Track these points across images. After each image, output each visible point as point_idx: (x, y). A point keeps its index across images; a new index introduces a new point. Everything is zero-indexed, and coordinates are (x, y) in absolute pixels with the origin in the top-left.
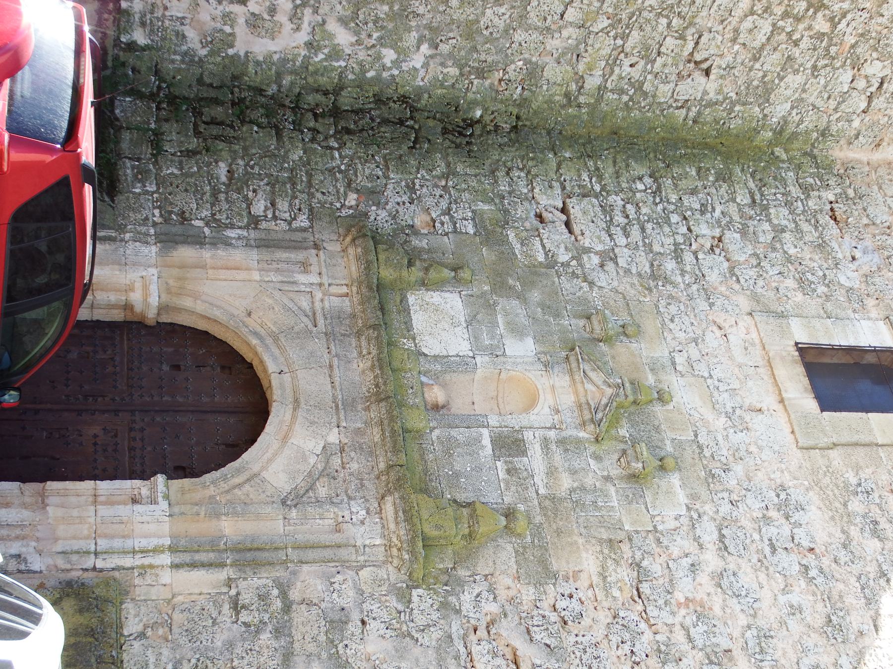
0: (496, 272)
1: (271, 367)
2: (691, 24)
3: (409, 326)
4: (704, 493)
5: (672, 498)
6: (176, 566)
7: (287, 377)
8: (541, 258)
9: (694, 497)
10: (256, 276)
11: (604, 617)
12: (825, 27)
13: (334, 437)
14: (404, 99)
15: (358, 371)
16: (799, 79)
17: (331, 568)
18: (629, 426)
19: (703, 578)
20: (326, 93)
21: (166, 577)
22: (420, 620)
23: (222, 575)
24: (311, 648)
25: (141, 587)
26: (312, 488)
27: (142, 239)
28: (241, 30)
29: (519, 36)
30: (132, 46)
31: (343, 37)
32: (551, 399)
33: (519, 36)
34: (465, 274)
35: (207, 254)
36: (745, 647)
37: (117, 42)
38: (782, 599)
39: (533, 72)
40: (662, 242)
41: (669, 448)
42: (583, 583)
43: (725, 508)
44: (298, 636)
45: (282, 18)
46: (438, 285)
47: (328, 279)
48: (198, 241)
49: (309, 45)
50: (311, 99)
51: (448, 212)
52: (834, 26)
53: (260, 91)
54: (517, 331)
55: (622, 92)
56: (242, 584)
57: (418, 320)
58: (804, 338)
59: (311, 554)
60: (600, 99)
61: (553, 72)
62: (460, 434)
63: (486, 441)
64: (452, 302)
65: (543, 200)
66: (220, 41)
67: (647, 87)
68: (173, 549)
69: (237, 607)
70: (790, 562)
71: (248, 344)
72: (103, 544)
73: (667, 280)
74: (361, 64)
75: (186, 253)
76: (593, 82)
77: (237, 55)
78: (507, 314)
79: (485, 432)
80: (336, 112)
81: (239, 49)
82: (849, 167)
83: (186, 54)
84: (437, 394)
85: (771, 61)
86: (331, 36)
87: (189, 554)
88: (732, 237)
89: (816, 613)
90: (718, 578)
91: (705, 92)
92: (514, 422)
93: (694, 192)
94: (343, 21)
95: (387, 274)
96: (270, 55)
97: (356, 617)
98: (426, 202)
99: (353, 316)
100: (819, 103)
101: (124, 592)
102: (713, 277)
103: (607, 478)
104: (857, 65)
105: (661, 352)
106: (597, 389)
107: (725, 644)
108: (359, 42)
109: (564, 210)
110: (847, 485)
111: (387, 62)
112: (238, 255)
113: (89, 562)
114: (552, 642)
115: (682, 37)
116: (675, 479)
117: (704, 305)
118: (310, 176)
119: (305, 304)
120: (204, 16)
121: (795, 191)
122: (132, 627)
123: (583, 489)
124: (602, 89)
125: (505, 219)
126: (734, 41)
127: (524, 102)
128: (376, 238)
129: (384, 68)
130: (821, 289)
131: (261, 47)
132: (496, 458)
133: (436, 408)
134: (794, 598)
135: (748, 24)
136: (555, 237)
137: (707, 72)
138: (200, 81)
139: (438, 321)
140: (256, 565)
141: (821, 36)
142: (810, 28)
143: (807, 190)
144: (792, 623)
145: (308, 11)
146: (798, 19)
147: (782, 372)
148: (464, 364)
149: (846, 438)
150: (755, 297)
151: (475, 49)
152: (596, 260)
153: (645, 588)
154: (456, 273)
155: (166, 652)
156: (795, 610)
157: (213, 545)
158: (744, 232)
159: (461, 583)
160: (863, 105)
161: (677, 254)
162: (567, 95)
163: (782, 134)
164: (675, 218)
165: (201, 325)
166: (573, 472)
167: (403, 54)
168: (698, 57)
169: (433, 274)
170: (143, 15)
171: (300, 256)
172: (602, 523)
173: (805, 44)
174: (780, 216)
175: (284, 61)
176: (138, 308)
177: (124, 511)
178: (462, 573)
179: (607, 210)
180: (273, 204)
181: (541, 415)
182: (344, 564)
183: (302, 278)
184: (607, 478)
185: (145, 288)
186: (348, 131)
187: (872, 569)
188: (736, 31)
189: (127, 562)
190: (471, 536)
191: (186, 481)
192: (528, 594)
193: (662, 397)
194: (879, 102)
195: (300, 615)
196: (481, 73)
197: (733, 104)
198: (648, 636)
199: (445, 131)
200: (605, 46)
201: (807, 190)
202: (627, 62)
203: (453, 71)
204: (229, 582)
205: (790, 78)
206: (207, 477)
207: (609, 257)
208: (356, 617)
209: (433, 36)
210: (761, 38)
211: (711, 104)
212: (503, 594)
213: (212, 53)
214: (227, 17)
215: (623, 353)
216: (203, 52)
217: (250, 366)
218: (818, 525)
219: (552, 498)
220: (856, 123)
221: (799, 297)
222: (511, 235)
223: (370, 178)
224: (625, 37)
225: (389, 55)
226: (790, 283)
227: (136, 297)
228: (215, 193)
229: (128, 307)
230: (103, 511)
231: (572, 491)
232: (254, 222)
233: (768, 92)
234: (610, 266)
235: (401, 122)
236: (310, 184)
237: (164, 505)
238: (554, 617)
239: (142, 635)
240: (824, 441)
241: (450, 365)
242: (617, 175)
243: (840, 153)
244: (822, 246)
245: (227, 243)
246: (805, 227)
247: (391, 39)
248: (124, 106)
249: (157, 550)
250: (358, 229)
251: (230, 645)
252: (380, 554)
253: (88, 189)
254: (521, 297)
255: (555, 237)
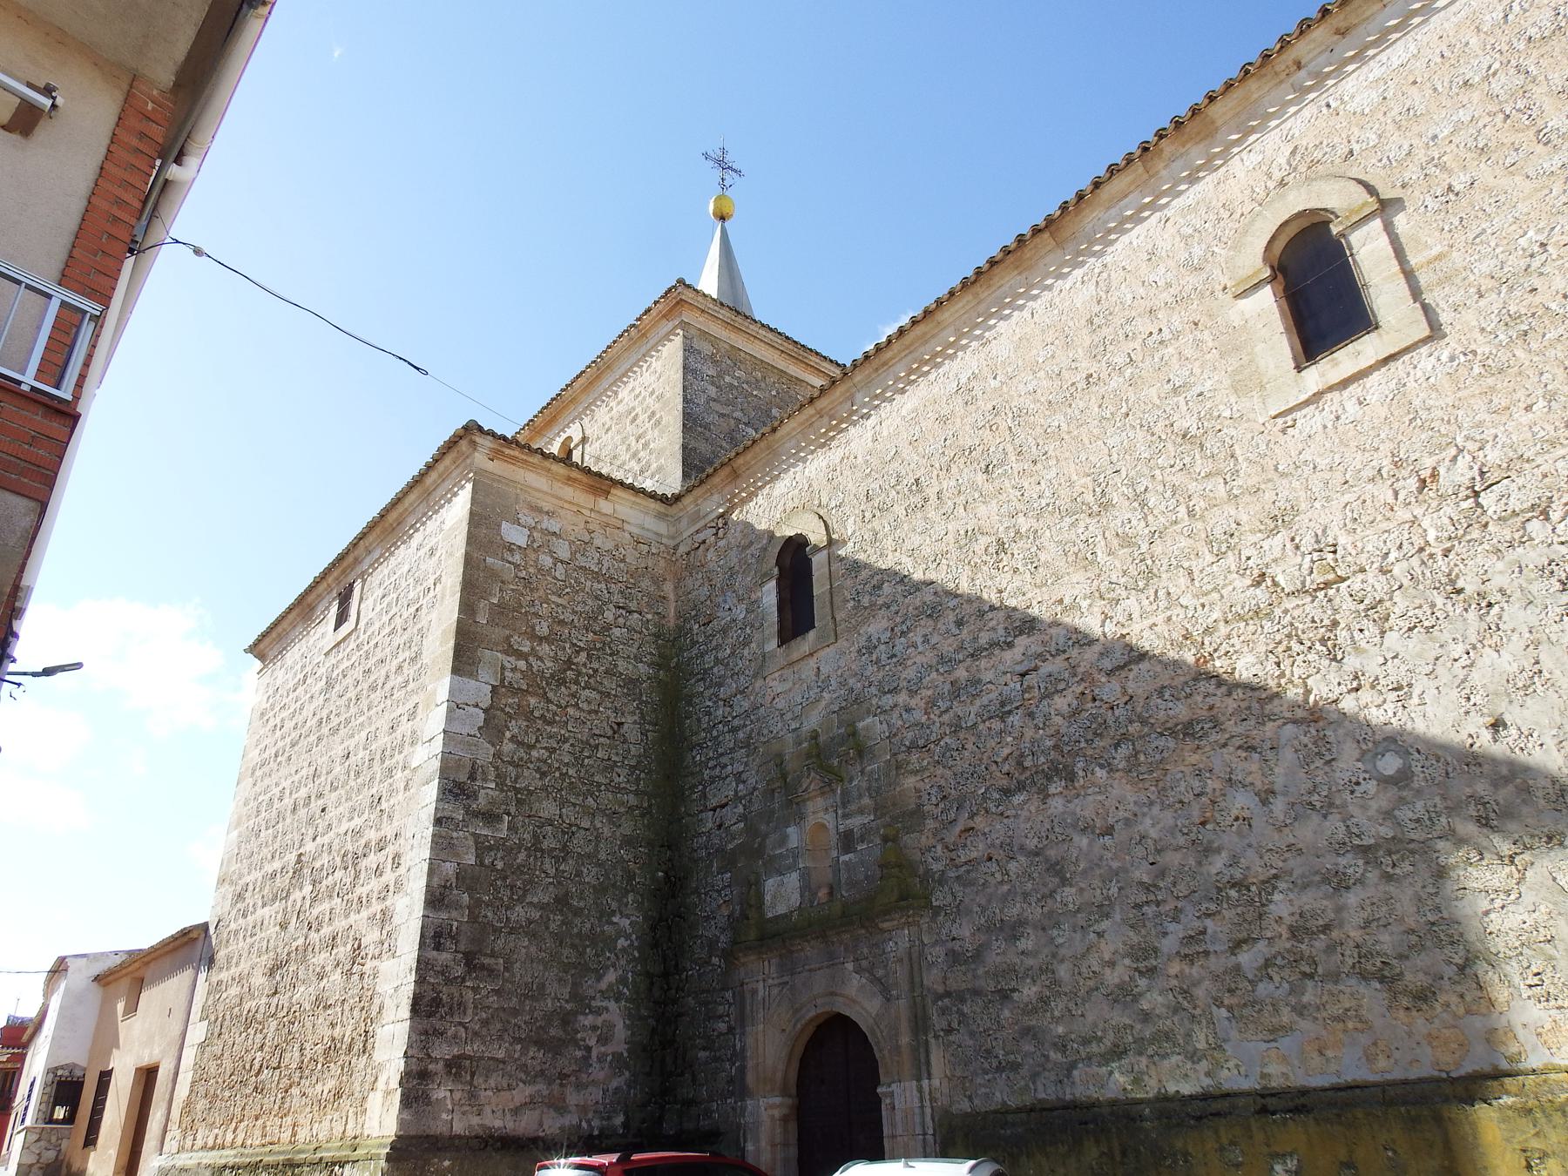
0: (751, 860)
1: (812, 1014)
2: (587, 743)
3: (785, 916)
4: (865, 706)
5: (872, 726)
6: (929, 1078)
7: (819, 1001)
8: (742, 825)
9: (868, 712)
10: (761, 1027)
11: (940, 771)
12: (583, 655)
13: (850, 966)
14: (653, 928)
15: (810, 950)
16: (620, 663)
17: (924, 964)
18: (834, 755)
19: (913, 703)
20: (652, 983)
21: (936, 1082)
22: (949, 898)
23: (932, 1041)
24: (969, 975)
25: (942, 1101)
26: (879, 980)
27: (743, 1109)
28: (609, 1049)
29: (603, 856)
30: (625, 1125)
31: (611, 977)
32: (820, 813)
33: (603, 856)
34: (752, 878)
35: (750, 1064)
36: (948, 672)
37: (623, 1136)
38: (921, 649)
39: (628, 842)
40: (728, 741)
41: (842, 730)
42: (920, 785)
43: (873, 690)
44: (964, 986)
45: (599, 1021)
46: (760, 896)
47: (761, 977)
48: (742, 1070)
49: (617, 1000)
50: (657, 993)
51: (719, 892)
52: (582, 649)
53: (654, 1031)
54: (784, 839)
55: (638, 779)
56: (937, 1027)
57: (781, 909)
58: (774, 643)
59: (917, 979)
60: (644, 793)
61: (627, 828)
62: (844, 876)
63: (846, 858)
64: (770, 884)
65: (710, 825)
66: (618, 1063)
67: (633, 763)
68: (919, 1080)
69: (950, 1031)
70: (901, 642)
71: (802, 1030)
72: (918, 1130)
73: (750, 737)
74: (629, 962)
75: (750, 1078)
76: (632, 800)
77: (628, 1050)
78: (774, 848)
79: (842, 858)
80: (666, 975)
81: (622, 1048)
82: (679, 616)
83: (629, 1087)
84: (822, 894)
85: (610, 684)
86: (610, 986)
87: (922, 1069)
88: (723, 692)
89: (926, 625)
90: (913, 693)
91: (635, 722)
92: (834, 838)
93: (699, 720)
94: (599, 979)
95: (753, 934)
96: (627, 1027)
97: (950, 945)
98: (715, 903)
99: (781, 956)
100: (636, 645)
101: (946, 1112)
102: (746, 705)
103: (862, 772)
104: (607, 628)
105: (790, 738)
106: (811, 782)
107: (948, 687)
108: (614, 965)
109: (714, 810)
110: (854, 608)
111: (626, 944)
112: (750, 1041)
113: (930, 1138)
114: (955, 806)
115: (597, 747)
116: (860, 725)
117: (762, 710)
118: (703, 992)
119: (775, 991)
120: (601, 1076)
121: (695, 651)
122: (965, 1106)
123: (869, 789)
124: (636, 793)
125: (720, 850)
126: (596, 712)
127: (650, 844)
128: (734, 942)
129: (631, 945)
130: (748, 631)
131: (621, 1032)
132: (855, 851)
133: (831, 894)
134: (919, 640)
135: (585, 706)
136: (731, 815)
137: (620, 724)
138: (649, 1074)
139: (783, 894)
140: (926, 1018)
141: (589, 657)
142: (585, 665)
143: (694, 643)
144: (933, 641)
145: (594, 1004)
146: (579, 674)
147: (795, 656)
148: (805, 876)
149: (828, 609)
150: (755, 676)
151: (614, 885)
152: (741, 786)
153: (921, 742)
154: (753, 887)
155: (979, 1080)
156: (926, 640)
157: (914, 1050)
158: (720, 685)
159: (928, 871)
160: (636, 616)
161: (734, 730)
162: (643, 815)
163: (661, 663)
164: (715, 733)
165: (795, 1065)
166: (860, 796)
167: (621, 933)
168: (610, 733)
169: (752, 902)
170: (603, 1119)
171: (748, 995)
172: (887, 775)
173: (595, 665)
174: (709, 659)
175: (630, 1016)
176: (785, 1111)
177: (899, 1116)
178: (921, 871)
179: (713, 780)
180: (721, 1017)
181: (828, 819)
182: (921, 954)
183: (761, 993)
184: (862, 772)
185: (772, 1107)
186: (677, 965)
187: (900, 588)
188: (590, 712)
189: (928, 1111)
190: (899, 866)
191: (881, 1071)
192: (931, 824)
193: (814, 736)
194: (633, 606)
195: (953, 985)
196: (631, 876)
197: (641, 702)
198: (947, 740)
199: (673, 896)
200: (606, 797)
201: (694, 643)
202: (617, 780)
203: (630, 897)
204: (936, 1037)
205: (620, 669)
206: (877, 1055)
207: (739, 778)
208: (950, 945)
209: (605, 915)
210: (594, 695)
211: (643, 716)
212: (932, 841)
213: (627, 1068)
214: (601, 1059)
215: (791, 765)
216: (627, 1074)
217: (819, 1027)
218: (877, 627)
219: (876, 810)
220: (649, 617)
221: (753, 645)
222: (730, 846)
223: (702, 948)
224: (599, 785)
225: (622, 943)
226: (746, 652)
227: (777, 1113)
228: (716, 1059)
229: (785, 1119)
230: (899, 1131)
231: (871, 797)
232: (731, 1030)
233: (631, 681)
234: (744, 776)
235: (669, 927)
236: (708, 991)
237: (894, 1086)
238: (942, 805)
239: (970, 1098)
240: (831, 625)
241: (807, 887)
242: (692, 774)
243: (671, 622)
244: (724, 631)
245: (743, 1049)
246: (714, 643)
247: (610, 943)
248: (669, 1128)
249: (920, 1090)
250: (729, 955)
251: (972, 1034)
252: (914, 929)
253: (614, 1158)
254: (766, 836)
255: (731, 815)
